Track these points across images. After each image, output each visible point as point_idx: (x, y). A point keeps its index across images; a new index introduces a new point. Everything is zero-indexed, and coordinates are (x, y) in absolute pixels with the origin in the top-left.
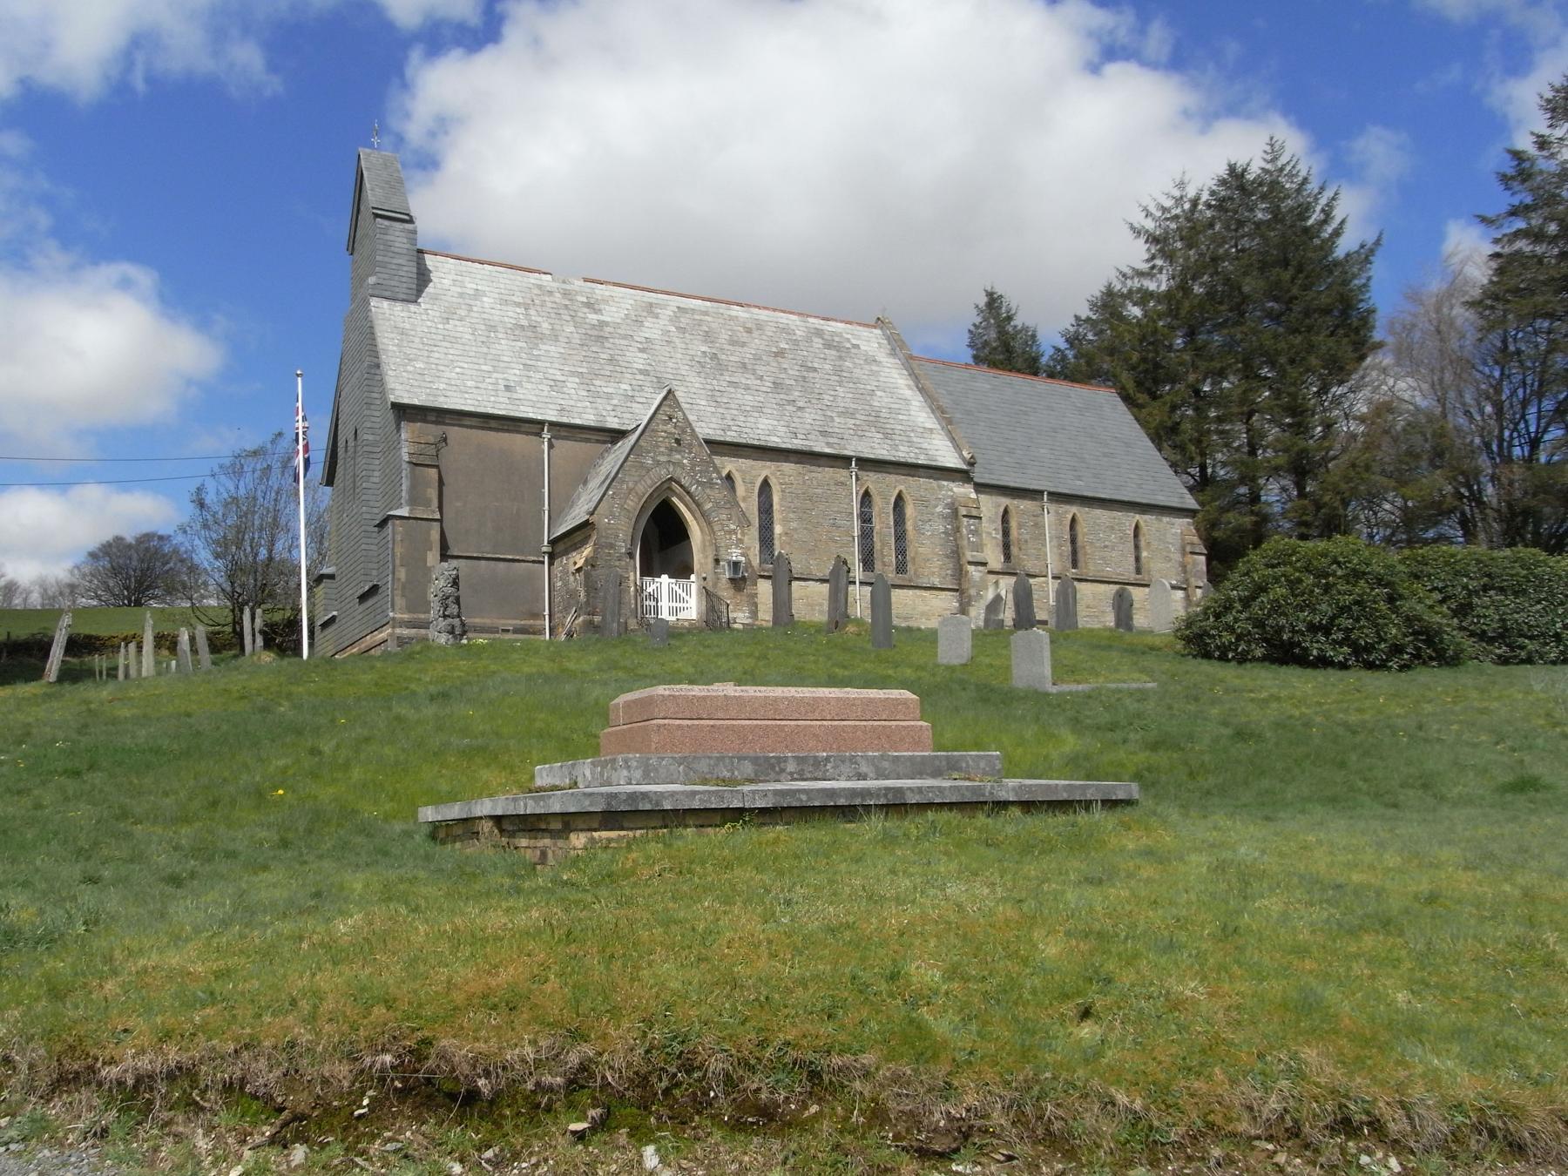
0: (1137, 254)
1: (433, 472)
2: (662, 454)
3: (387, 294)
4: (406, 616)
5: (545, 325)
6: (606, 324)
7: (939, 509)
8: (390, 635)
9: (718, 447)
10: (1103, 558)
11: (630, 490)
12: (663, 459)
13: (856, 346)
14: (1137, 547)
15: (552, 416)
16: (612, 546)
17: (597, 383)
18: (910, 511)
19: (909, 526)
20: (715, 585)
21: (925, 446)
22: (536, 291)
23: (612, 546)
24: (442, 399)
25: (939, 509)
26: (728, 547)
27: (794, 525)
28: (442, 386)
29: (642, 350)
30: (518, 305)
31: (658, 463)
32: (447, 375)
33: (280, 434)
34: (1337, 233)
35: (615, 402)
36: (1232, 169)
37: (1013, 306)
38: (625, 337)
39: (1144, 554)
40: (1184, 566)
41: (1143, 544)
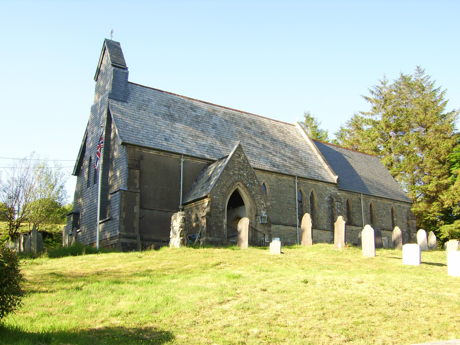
0: (368, 107)
1: (137, 172)
2: (236, 170)
3: (115, 98)
4: (125, 234)
5: (176, 115)
6: (199, 117)
7: (326, 198)
8: (118, 241)
9: (254, 168)
10: (381, 220)
11: (224, 185)
12: (237, 172)
13: (289, 132)
14: (393, 217)
15: (184, 152)
16: (217, 208)
17: (199, 140)
18: (316, 198)
19: (316, 205)
20: (256, 226)
21: (320, 173)
22: (171, 101)
23: (217, 208)
24: (141, 142)
25: (326, 198)
26: (260, 211)
27: (274, 202)
28: (141, 137)
29: (213, 128)
30: (166, 106)
31: (234, 174)
32: (142, 132)
33: (34, 152)
34: (445, 104)
35: (207, 148)
36: (403, 78)
37: (319, 121)
38: (206, 122)
39: (395, 219)
40: (408, 224)
41: (394, 215)
